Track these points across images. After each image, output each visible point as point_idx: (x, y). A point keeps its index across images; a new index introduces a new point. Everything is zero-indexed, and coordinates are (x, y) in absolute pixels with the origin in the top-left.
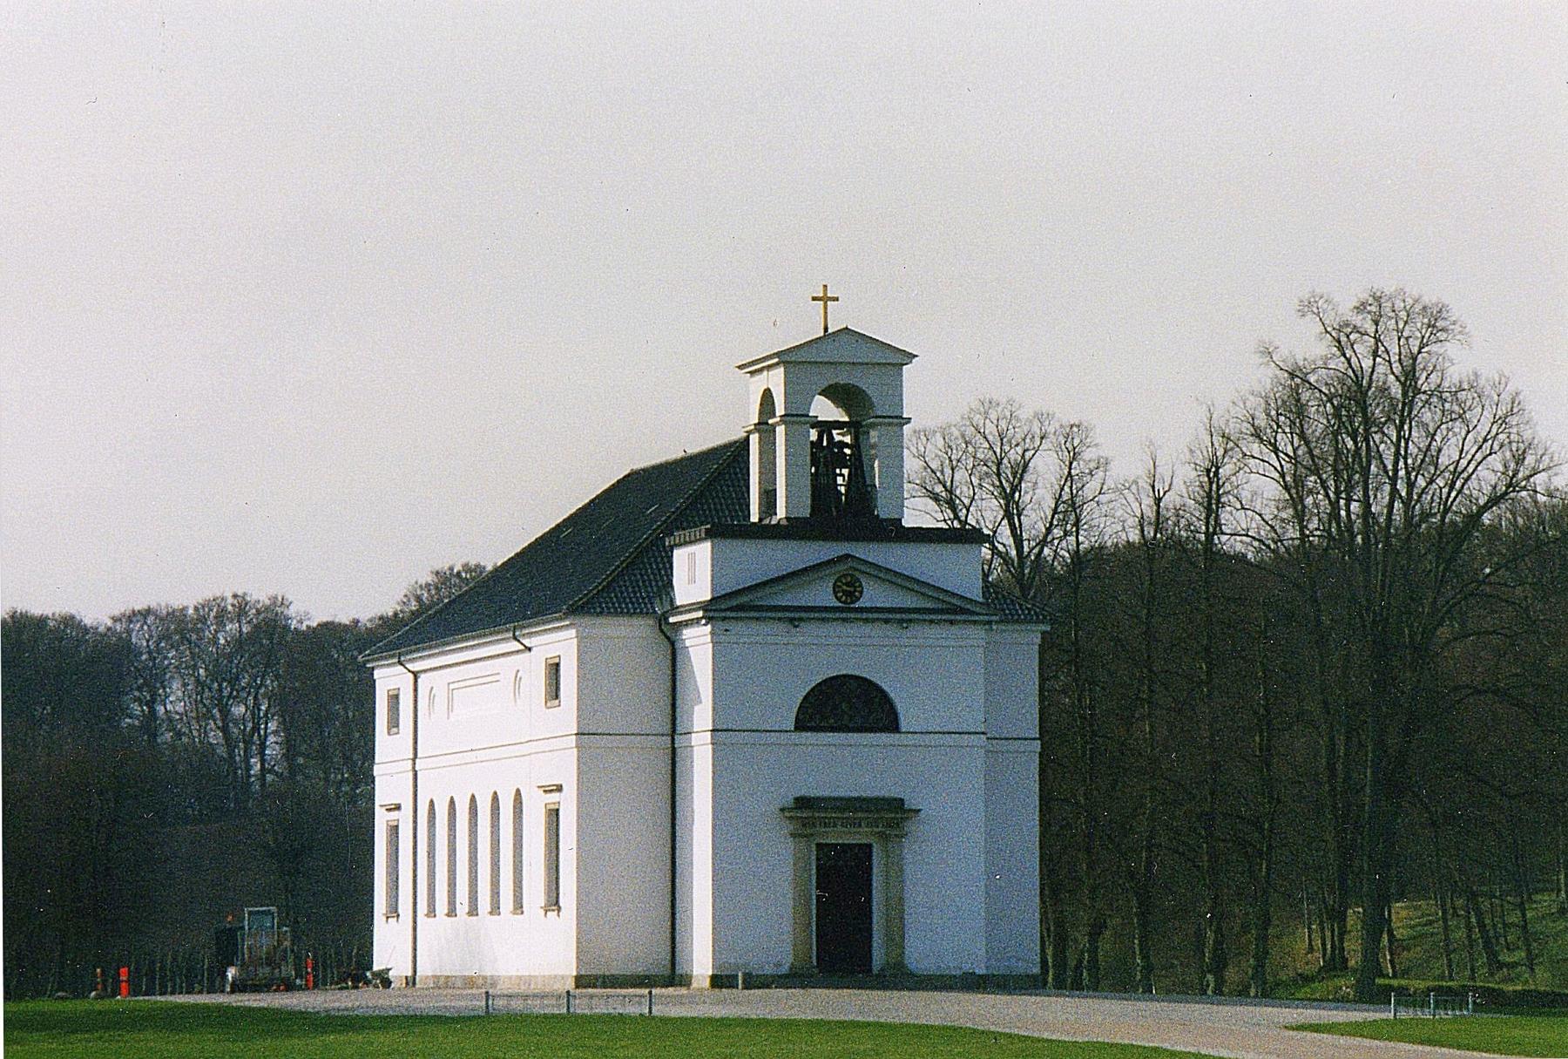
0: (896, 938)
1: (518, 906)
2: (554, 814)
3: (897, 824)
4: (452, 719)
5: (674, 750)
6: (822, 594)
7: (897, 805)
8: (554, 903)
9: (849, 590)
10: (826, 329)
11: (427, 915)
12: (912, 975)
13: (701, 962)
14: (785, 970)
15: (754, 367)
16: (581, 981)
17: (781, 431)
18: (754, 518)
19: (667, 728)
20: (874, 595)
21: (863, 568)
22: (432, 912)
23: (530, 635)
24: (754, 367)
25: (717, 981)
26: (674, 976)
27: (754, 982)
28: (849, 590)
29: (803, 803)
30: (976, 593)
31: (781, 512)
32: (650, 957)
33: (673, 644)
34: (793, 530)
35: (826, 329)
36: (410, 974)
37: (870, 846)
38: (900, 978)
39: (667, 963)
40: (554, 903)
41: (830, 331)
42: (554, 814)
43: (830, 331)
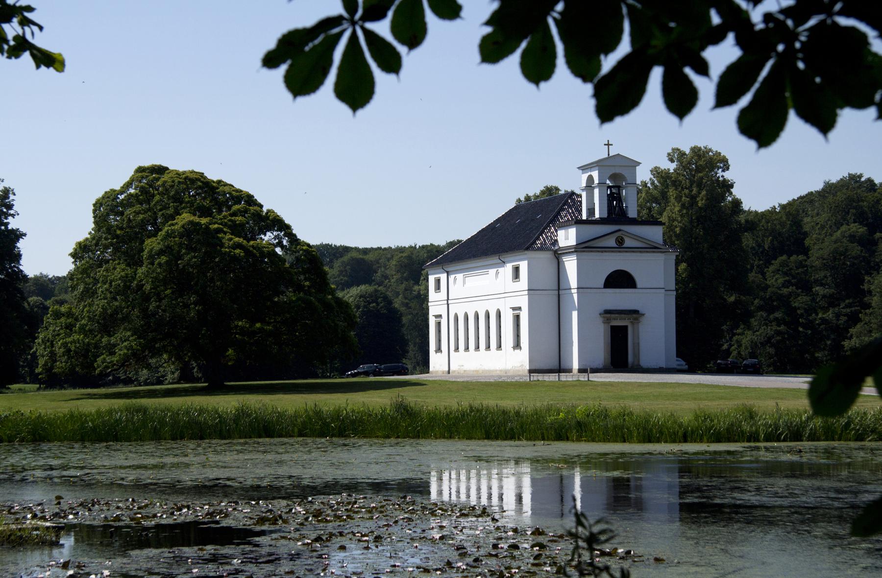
0: (637, 355)
1: (499, 347)
2: (517, 318)
3: (636, 319)
4: (466, 285)
5: (559, 295)
6: (611, 242)
7: (636, 312)
8: (517, 345)
9: (620, 241)
10: (609, 155)
11: (436, 352)
12: (642, 368)
13: (576, 366)
14: (601, 366)
15: (584, 168)
16: (531, 371)
17: (596, 191)
18: (584, 217)
19: (556, 288)
20: (628, 242)
21: (626, 234)
22: (457, 349)
23: (504, 258)
24: (584, 168)
25: (581, 371)
26: (560, 369)
27: (595, 371)
28: (620, 241)
29: (607, 312)
30: (661, 242)
31: (597, 215)
32: (553, 363)
33: (558, 260)
34: (602, 221)
35: (609, 155)
36: (447, 369)
37: (626, 327)
38: (638, 369)
39: (558, 365)
40: (517, 345)
41: (610, 155)
42: (517, 318)
43: (610, 155)
